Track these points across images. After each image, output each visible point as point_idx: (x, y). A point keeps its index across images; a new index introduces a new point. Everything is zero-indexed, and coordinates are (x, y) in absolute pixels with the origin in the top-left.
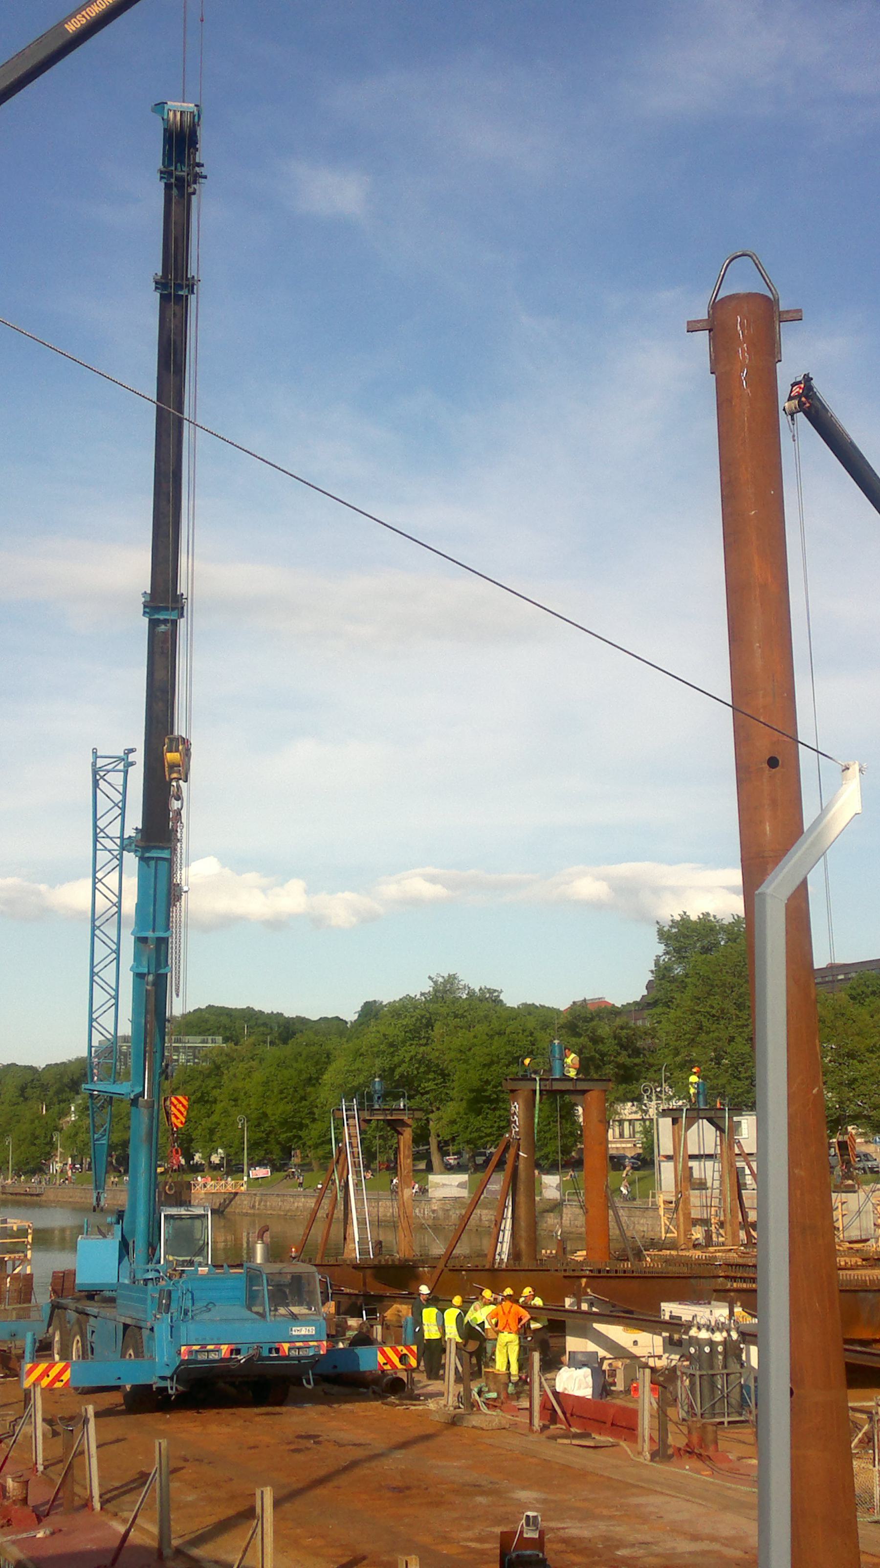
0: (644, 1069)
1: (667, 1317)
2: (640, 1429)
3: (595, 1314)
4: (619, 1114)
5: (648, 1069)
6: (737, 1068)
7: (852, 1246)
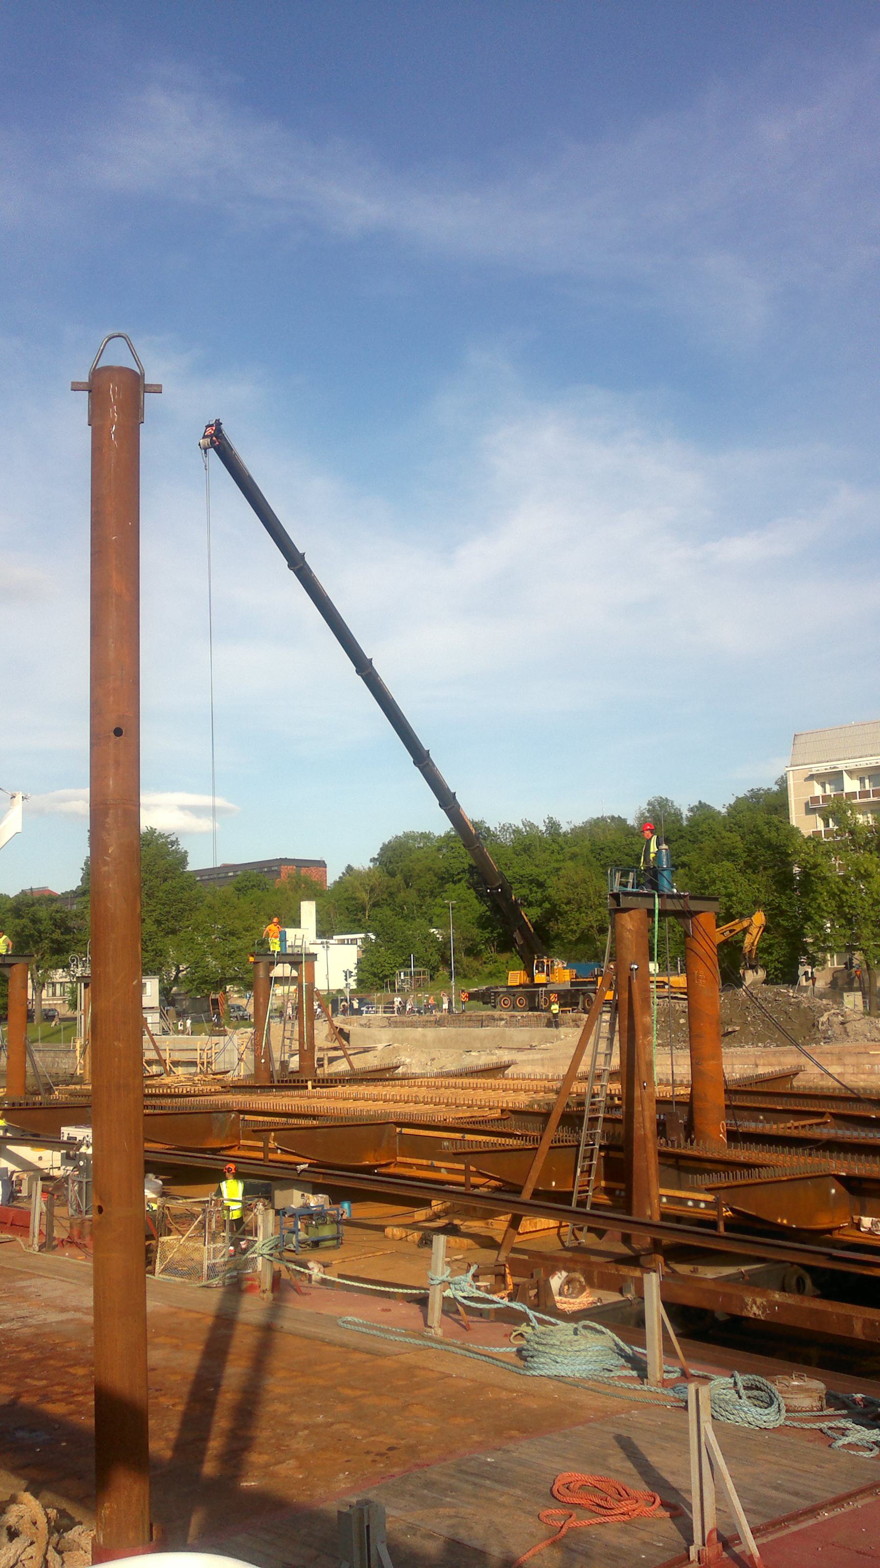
0: (73, 944)
1: (65, 1138)
2: (31, 1228)
3: (9, 1138)
4: (51, 978)
5: (76, 943)
6: (145, 943)
7: (215, 1077)
